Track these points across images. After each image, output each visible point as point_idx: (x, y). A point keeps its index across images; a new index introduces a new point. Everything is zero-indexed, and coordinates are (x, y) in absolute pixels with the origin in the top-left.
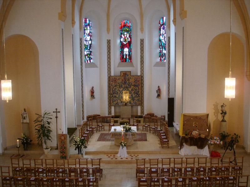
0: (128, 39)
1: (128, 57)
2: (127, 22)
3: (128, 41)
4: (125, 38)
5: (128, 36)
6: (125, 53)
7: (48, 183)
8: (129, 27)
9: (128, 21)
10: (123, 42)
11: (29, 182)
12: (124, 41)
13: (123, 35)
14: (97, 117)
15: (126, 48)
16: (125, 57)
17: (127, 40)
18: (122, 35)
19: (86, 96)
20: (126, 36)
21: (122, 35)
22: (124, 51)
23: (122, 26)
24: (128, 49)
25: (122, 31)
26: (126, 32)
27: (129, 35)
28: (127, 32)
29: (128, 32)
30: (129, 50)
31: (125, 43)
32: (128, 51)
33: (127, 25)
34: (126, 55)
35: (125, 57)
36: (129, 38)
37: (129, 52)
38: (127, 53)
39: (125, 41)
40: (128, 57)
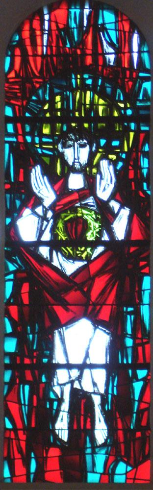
0: (106, 216)
1: (101, 432)
2: (97, 29)
3: (113, 245)
4: (67, 202)
5: (105, 188)
6: (62, 376)
7: (106, 238)
8: (121, 78)
9: (108, 18)
10: (44, 251)
11: (29, 139)
12: (55, 245)
13: (48, 171)
14: (114, 422)
15: (84, 324)
16: (62, 427)
17: (95, 226)
18: (36, 173)
19: (43, 187)
20: (76, 182)
21: (36, 173)
22: (59, 357)
23: (36, 65)
24: (102, 339)
25: (37, 122)
26: (80, 133)
27: (120, 176)
28: (92, 138)
29: (100, 132)
30: (116, 347)
31: (70, 268)
32: (100, 356)
33: (98, 53)
34: (81, 402)
35: (62, 427)
36: (115, 205)
37: (114, 368)
38: (96, 382)
39: (73, 238)
40: (101, 432)
